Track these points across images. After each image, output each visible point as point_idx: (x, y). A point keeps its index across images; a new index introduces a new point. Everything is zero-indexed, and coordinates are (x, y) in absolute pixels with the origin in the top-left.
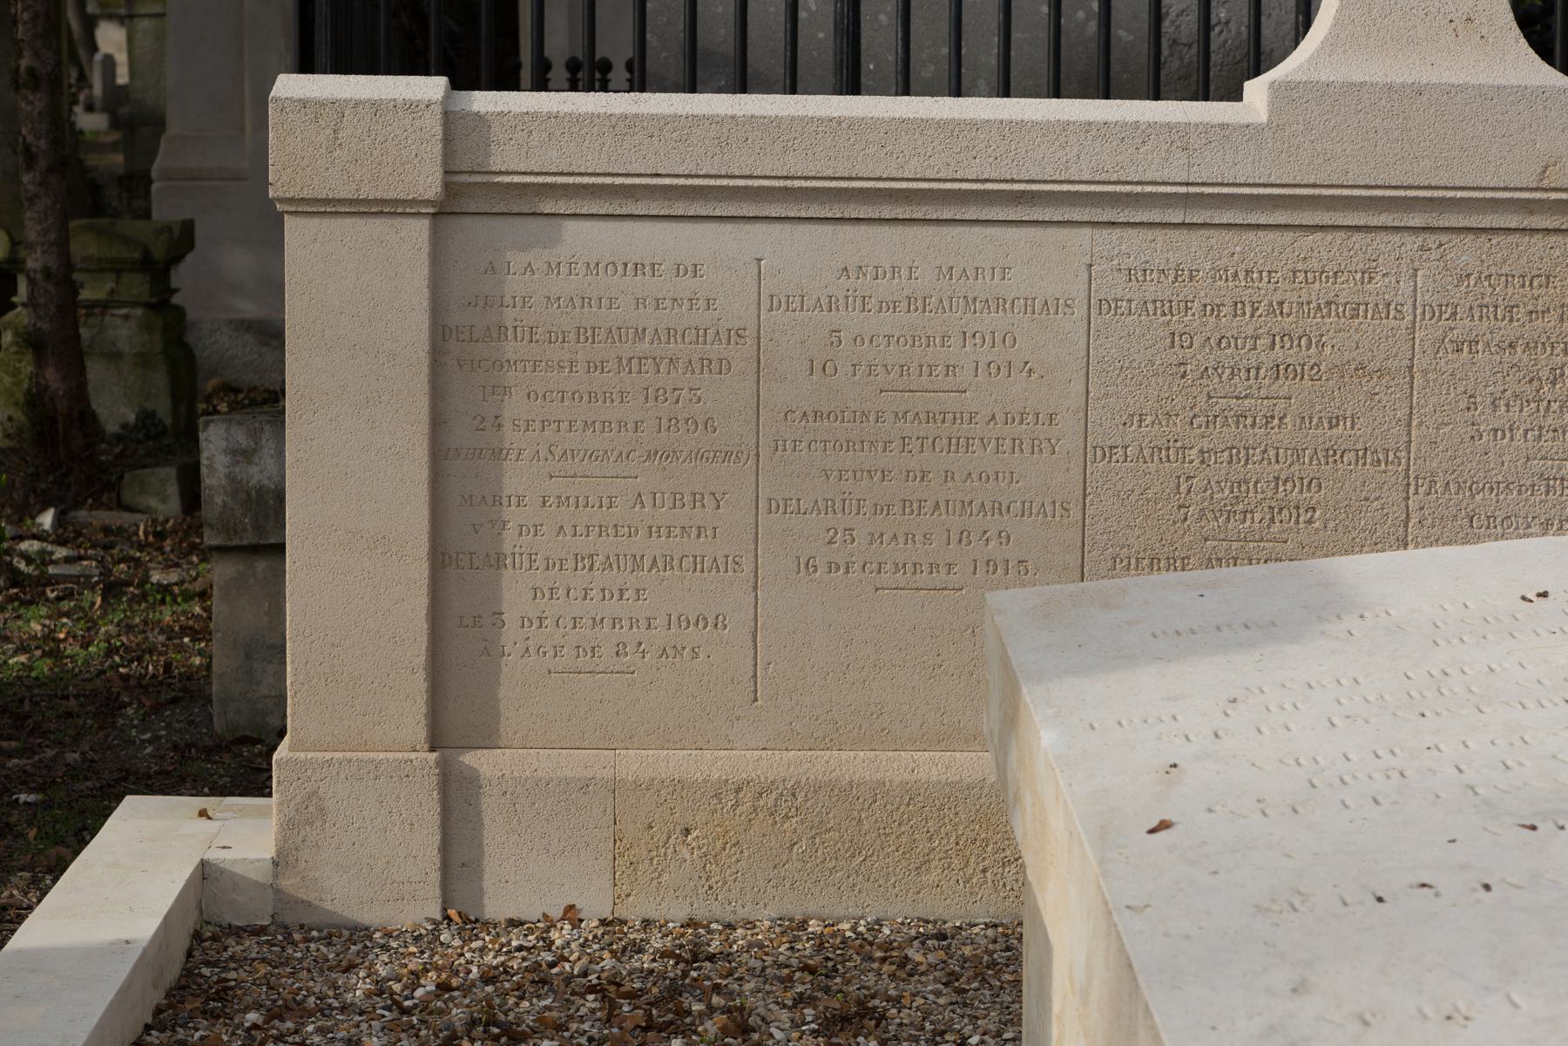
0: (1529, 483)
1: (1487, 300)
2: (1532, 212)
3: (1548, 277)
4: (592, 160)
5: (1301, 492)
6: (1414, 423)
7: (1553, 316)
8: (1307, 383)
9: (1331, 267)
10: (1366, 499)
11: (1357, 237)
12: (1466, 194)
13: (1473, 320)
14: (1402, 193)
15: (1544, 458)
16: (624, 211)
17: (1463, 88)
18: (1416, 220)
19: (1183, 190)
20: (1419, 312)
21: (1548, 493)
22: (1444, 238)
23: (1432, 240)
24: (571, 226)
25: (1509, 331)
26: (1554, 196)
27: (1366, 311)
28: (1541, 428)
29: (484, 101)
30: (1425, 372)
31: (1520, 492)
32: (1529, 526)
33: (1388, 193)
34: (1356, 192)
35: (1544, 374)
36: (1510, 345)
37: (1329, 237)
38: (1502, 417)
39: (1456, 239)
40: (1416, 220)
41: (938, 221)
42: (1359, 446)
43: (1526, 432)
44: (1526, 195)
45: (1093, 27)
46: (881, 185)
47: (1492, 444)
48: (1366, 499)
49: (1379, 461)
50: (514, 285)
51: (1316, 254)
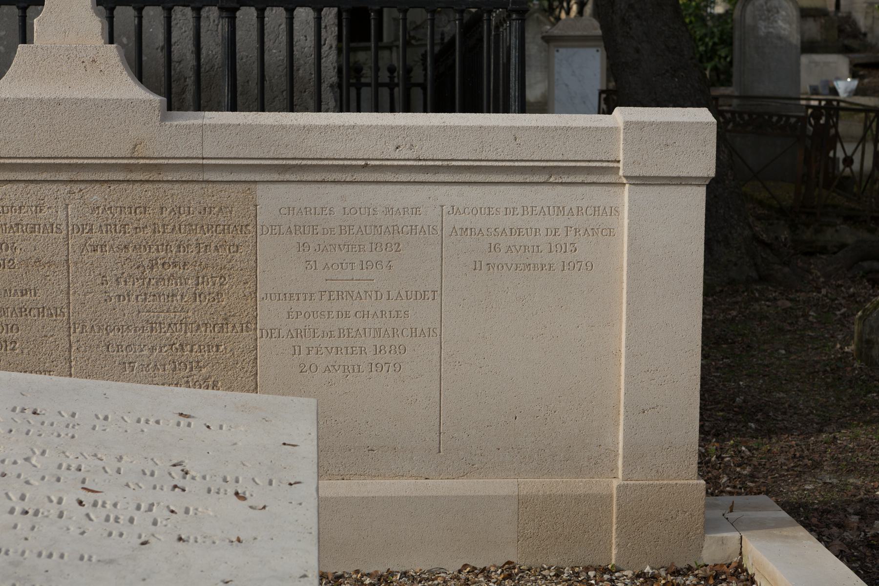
0: (140, 325)
1: (110, 221)
2: (131, 171)
3: (145, 208)
5: (7, 332)
6: (71, 292)
7: (149, 230)
8: (7, 270)
9: (17, 204)
10: (45, 336)
11: (31, 186)
12: (89, 161)
13: (102, 233)
14: (52, 161)
15: (148, 311)
16: (569, 180)
17: (84, 100)
18: (64, 176)
19: (200, 162)
20: (70, 229)
21: (152, 331)
22: (82, 186)
23: (76, 188)
25: (124, 239)
26: (142, 161)
27: (39, 229)
28: (145, 294)
30: (76, 263)
31: (135, 331)
32: (142, 351)
33: (43, 161)
34: (25, 161)
35: (146, 263)
36: (125, 247)
37: (15, 187)
38: (122, 289)
39: (89, 187)
40: (64, 176)
42: (39, 306)
44: (126, 161)
46: (516, 164)
47: (117, 304)
48: (45, 336)
49: (52, 314)
51: (7, 196)
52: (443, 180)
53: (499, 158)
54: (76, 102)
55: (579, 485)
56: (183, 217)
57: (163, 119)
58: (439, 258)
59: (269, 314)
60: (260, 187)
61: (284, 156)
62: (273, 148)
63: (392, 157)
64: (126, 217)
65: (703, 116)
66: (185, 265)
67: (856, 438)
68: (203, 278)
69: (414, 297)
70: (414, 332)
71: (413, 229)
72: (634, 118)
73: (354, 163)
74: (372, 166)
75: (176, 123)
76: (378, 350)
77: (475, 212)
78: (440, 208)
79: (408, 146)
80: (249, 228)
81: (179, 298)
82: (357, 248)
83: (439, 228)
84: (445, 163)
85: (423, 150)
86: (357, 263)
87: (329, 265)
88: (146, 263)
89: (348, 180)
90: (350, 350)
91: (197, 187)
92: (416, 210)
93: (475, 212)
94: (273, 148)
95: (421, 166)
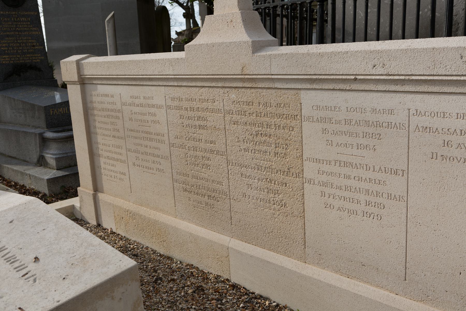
7: (254, 115)
17: (223, 43)
18: (220, 85)
22: (228, 90)
24: (98, 86)
35: (254, 133)
40: (220, 85)
41: (159, 85)
43: (252, 150)
45: (429, 13)
52: (408, 90)
53: (447, 73)
56: (268, 109)
57: (253, 53)
58: (407, 147)
59: (310, 170)
60: (302, 92)
61: (309, 73)
62: (304, 68)
63: (371, 73)
64: (246, 107)
66: (270, 136)
68: (278, 144)
69: (390, 172)
70: (389, 196)
71: (389, 125)
73: (321, 77)
74: (360, 79)
75: (259, 54)
76: (368, 204)
77: (433, 115)
78: (407, 111)
79: (381, 65)
80: (298, 117)
81: (268, 154)
82: (355, 135)
83: (407, 126)
84: (407, 78)
85: (391, 68)
86: (355, 145)
87: (339, 144)
88: (254, 133)
89: (347, 89)
90: (351, 200)
91: (274, 91)
92: (391, 112)
93: (433, 115)
94: (304, 68)
95: (390, 79)
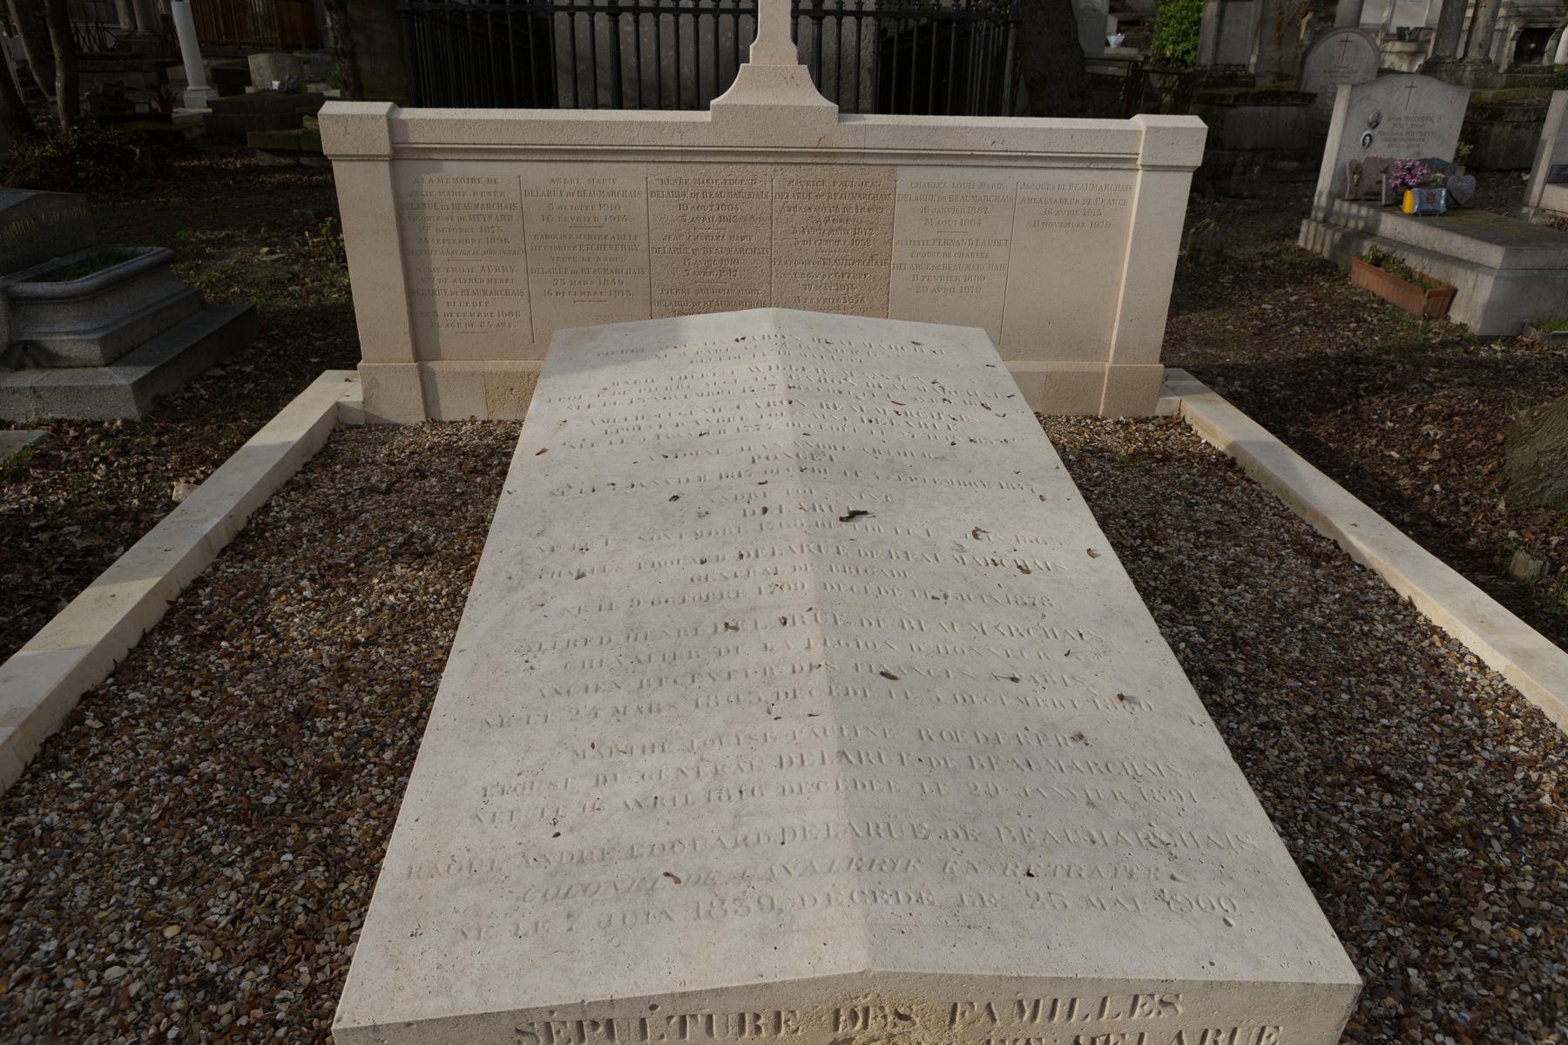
4: (448, 138)
18: (771, 160)
23: (778, 168)
29: (408, 113)
40: (771, 160)
50: (426, 187)
54: (783, 108)
55: (1085, 366)
65: (1194, 123)
67: (1202, 320)
72: (1153, 124)
